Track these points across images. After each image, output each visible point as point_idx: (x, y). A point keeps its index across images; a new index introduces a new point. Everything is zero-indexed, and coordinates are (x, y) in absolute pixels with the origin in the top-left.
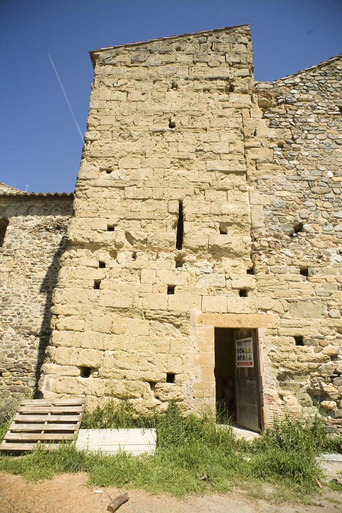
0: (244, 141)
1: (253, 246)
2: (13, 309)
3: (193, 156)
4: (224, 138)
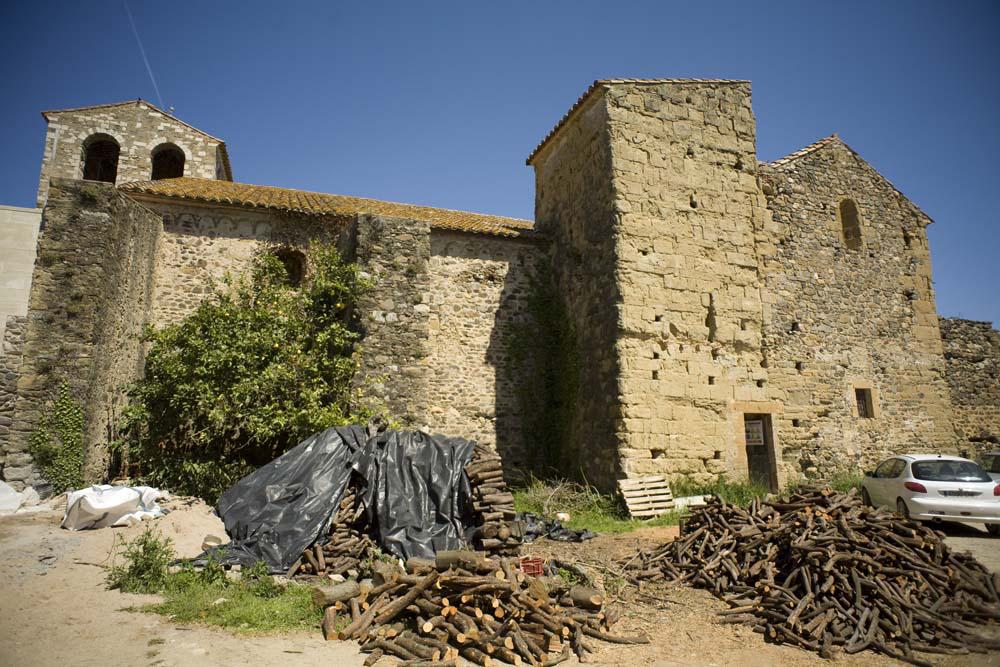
0: (753, 232)
1: (763, 342)
2: (452, 384)
3: (715, 246)
4: (739, 228)
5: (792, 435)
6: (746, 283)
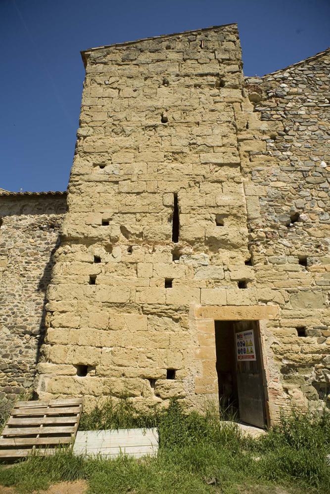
0: (236, 133)
2: (7, 308)
5: (296, 347)
6: (223, 179)
